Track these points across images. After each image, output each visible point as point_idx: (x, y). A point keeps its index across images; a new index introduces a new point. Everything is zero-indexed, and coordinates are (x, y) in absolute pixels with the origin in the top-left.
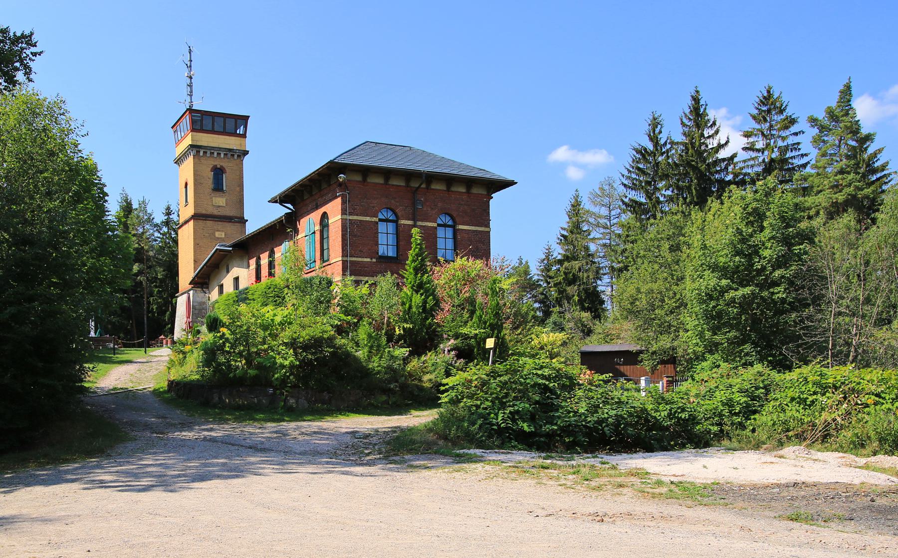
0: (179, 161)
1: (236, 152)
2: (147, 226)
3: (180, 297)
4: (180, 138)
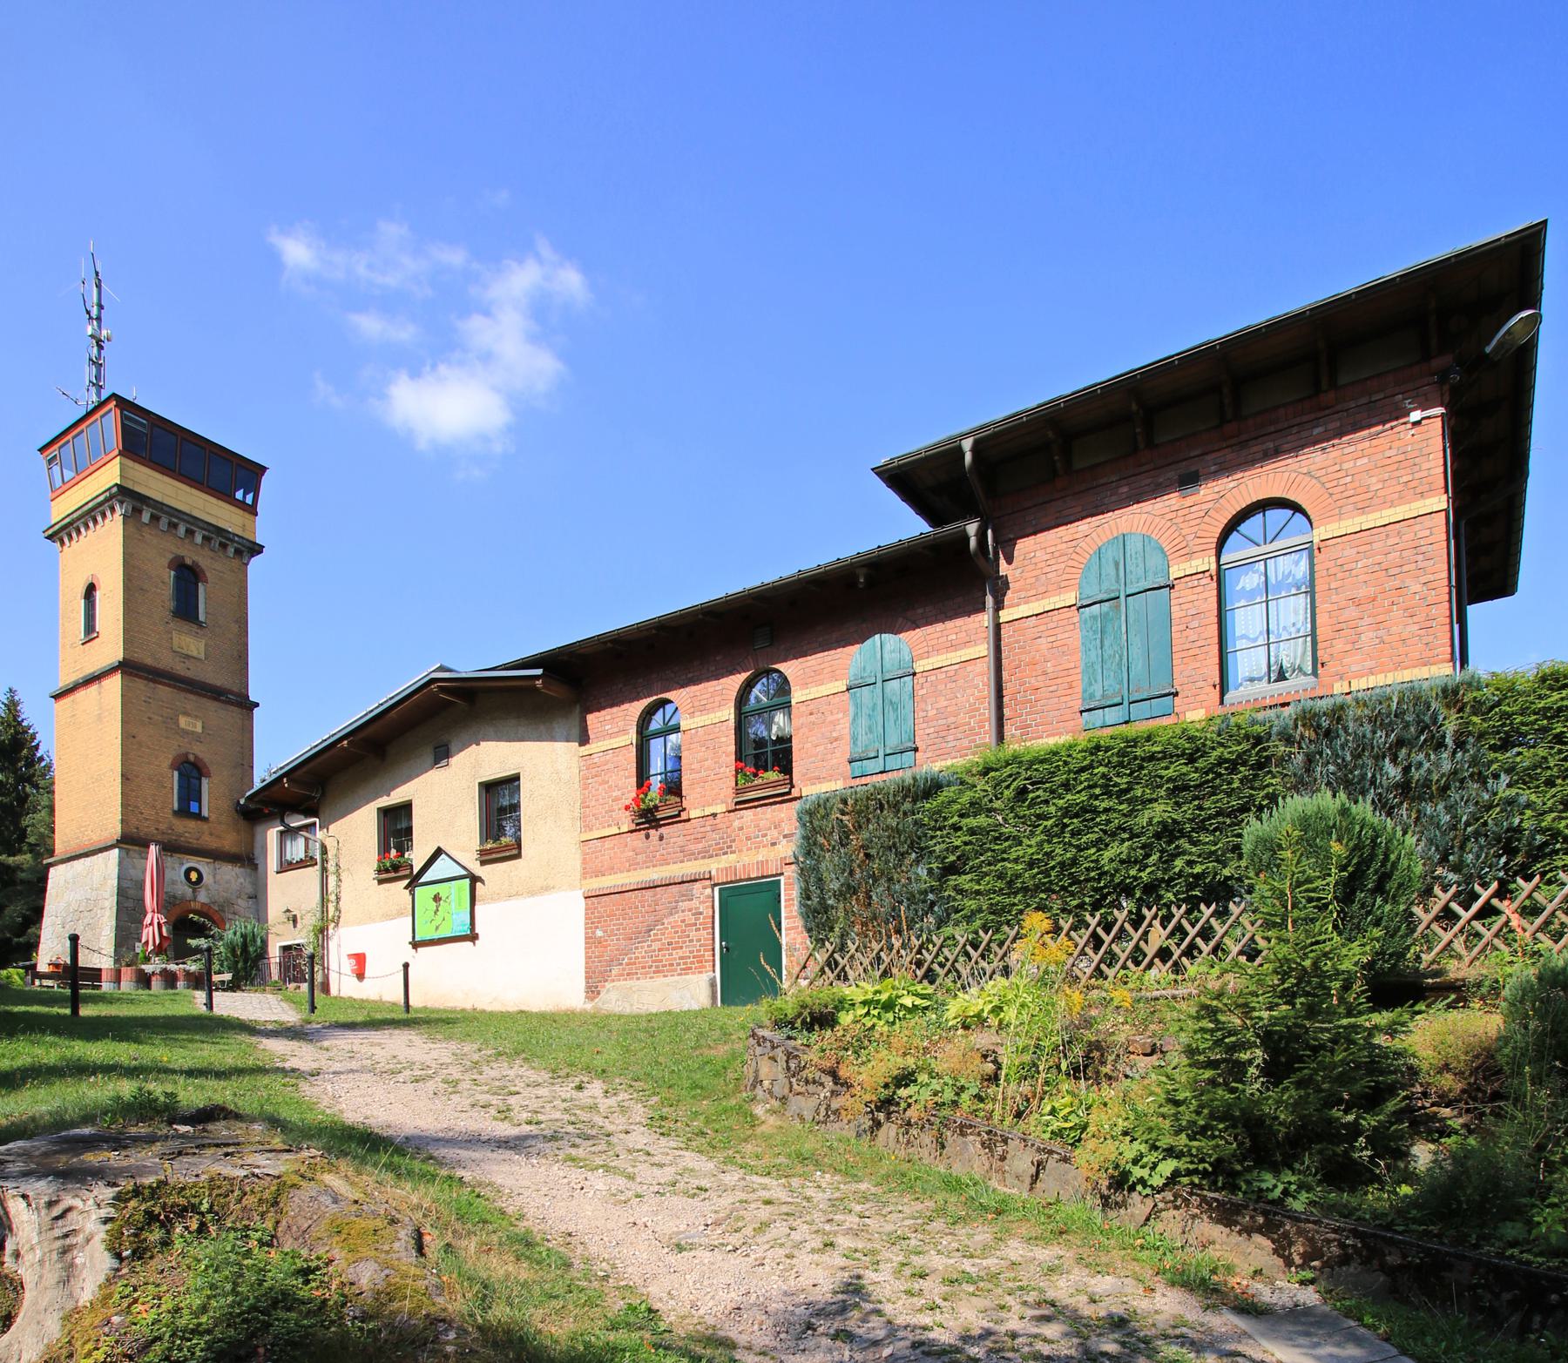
0: (61, 534)
1: (232, 541)
3: (61, 867)
4: (58, 483)
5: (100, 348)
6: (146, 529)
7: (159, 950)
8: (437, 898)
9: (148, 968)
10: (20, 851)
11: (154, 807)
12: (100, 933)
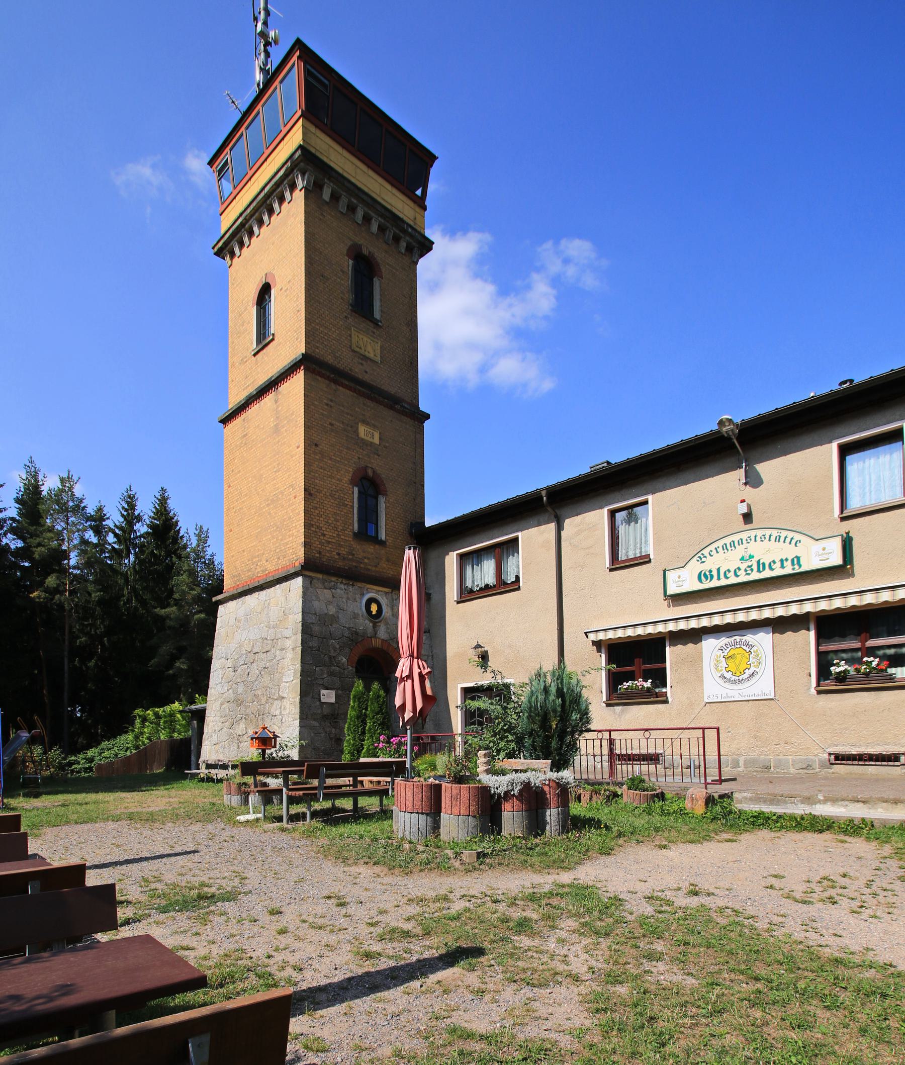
3: (231, 605)
10: (168, 605)
11: (335, 528)
12: (280, 679)
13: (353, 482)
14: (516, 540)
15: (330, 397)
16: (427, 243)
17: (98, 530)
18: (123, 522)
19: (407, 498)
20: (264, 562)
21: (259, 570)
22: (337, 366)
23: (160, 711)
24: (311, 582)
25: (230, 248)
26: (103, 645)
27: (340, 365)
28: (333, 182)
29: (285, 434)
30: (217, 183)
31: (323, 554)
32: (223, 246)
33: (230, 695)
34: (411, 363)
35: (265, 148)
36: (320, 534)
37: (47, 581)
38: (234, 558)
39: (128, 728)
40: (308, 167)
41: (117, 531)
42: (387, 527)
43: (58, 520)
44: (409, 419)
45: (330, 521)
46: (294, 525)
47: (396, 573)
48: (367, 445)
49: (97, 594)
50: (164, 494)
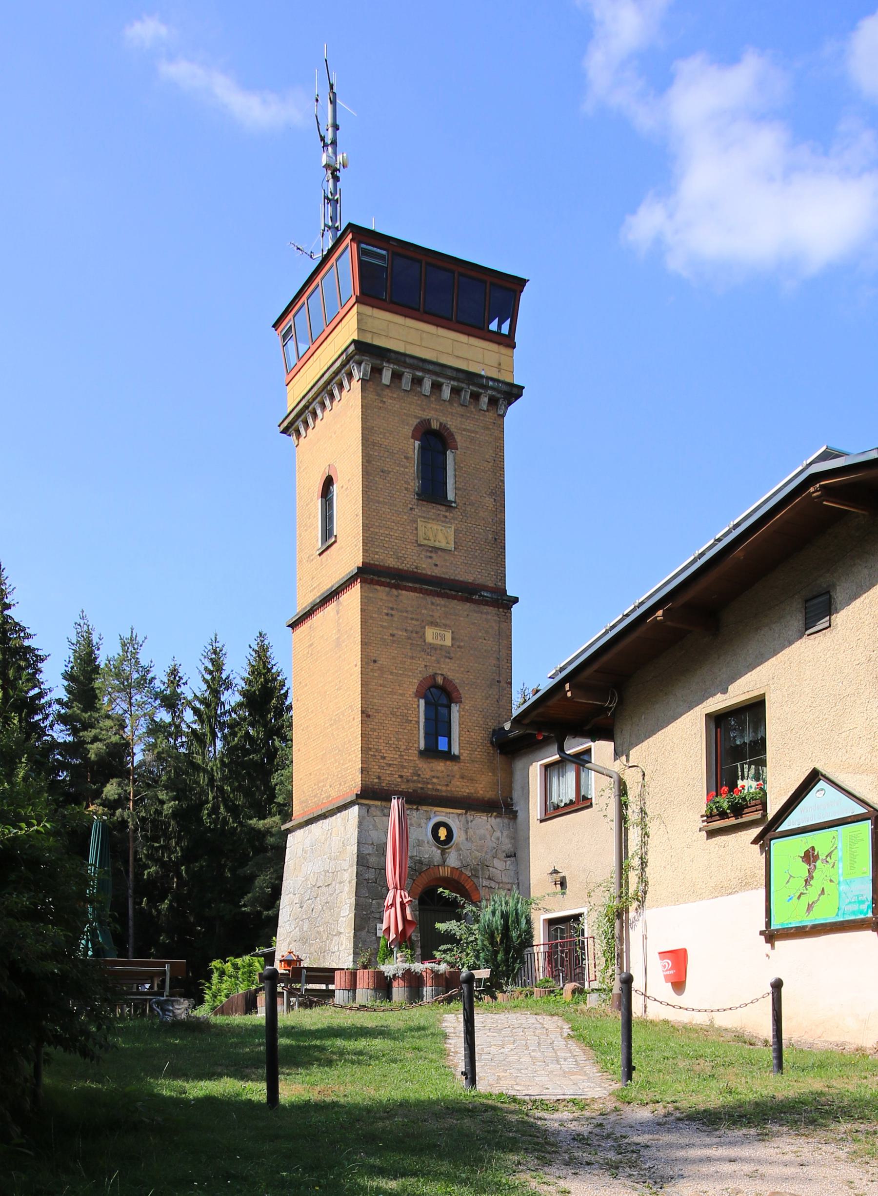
1: (486, 387)
2: (138, 697)
3: (299, 833)
4: (293, 359)
5: (336, 179)
6: (387, 392)
7: (403, 940)
8: (810, 857)
9: (389, 968)
10: (271, 814)
11: (397, 749)
13: (419, 694)
14: (588, 751)
15: (391, 605)
16: (515, 391)
17: (171, 702)
18: (206, 691)
19: (488, 701)
20: (328, 787)
21: (324, 796)
22: (400, 567)
23: (239, 961)
24: (368, 811)
25: (295, 428)
26: (179, 875)
27: (404, 565)
28: (392, 363)
29: (346, 650)
30: (282, 349)
31: (382, 778)
32: (289, 425)
33: (297, 933)
34: (495, 539)
35: (325, 326)
36: (379, 757)
37: (105, 790)
38: (302, 782)
39: (204, 984)
40: (363, 357)
41: (197, 704)
42: (461, 738)
43: (118, 701)
44: (491, 608)
45: (391, 742)
46: (353, 749)
47: (473, 791)
48: (436, 649)
49: (170, 805)
50: (263, 641)
